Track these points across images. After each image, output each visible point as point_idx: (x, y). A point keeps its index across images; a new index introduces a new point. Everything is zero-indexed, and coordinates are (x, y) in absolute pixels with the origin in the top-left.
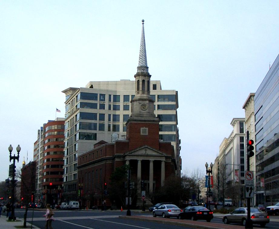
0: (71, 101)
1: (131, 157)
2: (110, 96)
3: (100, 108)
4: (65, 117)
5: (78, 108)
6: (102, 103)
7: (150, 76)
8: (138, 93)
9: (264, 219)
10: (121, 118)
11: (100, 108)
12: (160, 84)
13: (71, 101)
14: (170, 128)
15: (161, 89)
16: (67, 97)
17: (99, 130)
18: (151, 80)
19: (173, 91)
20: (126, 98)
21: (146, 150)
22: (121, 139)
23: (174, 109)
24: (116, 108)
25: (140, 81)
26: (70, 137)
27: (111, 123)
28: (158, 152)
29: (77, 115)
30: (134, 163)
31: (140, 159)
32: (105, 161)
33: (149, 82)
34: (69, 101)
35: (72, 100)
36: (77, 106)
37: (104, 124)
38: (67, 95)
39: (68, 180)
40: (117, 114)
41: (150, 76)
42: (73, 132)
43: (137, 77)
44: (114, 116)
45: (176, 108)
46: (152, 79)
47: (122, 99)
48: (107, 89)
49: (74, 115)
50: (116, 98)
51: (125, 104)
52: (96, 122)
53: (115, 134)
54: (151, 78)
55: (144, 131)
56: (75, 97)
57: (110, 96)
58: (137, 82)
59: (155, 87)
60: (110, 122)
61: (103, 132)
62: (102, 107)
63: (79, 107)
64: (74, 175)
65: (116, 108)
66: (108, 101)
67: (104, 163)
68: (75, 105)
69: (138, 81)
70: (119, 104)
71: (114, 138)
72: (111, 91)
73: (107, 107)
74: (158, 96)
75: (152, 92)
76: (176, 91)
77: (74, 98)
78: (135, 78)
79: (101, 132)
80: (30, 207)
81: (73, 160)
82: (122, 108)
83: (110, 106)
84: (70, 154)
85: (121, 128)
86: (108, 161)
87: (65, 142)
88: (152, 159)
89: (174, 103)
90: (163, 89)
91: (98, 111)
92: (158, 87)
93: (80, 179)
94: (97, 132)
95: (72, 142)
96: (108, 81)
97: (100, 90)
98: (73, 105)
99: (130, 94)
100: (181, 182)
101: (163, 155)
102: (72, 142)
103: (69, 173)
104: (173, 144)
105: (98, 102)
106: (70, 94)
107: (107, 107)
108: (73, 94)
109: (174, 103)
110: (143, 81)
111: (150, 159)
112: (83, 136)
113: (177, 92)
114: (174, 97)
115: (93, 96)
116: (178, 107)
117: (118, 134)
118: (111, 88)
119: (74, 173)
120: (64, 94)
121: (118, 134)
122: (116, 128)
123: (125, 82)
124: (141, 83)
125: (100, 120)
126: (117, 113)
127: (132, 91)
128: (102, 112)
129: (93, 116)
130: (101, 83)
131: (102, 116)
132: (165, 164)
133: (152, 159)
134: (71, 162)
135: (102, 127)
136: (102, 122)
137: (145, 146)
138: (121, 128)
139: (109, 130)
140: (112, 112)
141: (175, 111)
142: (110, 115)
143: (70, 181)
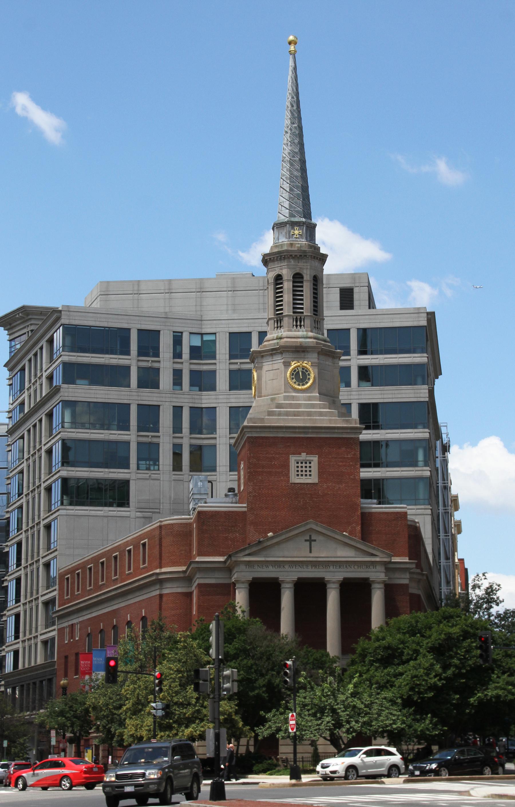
0: (33, 352)
1: (256, 568)
3: (141, 384)
4: (7, 421)
5: (54, 385)
6: (149, 365)
7: (323, 258)
9: (242, 473)
10: (223, 420)
11: (141, 384)
12: (369, 287)
14: (407, 454)
15: (371, 304)
16: (13, 343)
18: (325, 272)
19: (418, 311)
20: (240, 343)
21: (310, 541)
22: (219, 502)
23: (419, 380)
24: (203, 381)
25: (285, 278)
26: (29, 569)
27: (186, 440)
29: (52, 410)
31: (288, 577)
32: (158, 586)
33: (317, 281)
35: (31, 355)
36: (50, 378)
37: (158, 444)
38: (13, 337)
39: (20, 667)
40: (203, 406)
41: (323, 258)
42: (41, 442)
43: (271, 265)
44: (197, 412)
45: (432, 375)
46: (329, 268)
47: (222, 348)
48: (167, 310)
49: (41, 412)
51: (234, 367)
52: (125, 438)
53: (196, 482)
54: (325, 267)
58: (272, 281)
59: (347, 299)
60: (179, 435)
62: (149, 379)
63: (58, 380)
64: (45, 643)
65: (203, 381)
66: (228, 356)
67: (157, 592)
68: (45, 375)
69: (278, 278)
70: (212, 367)
71: (195, 497)
73: (166, 379)
74: (363, 333)
75: (334, 317)
76: (428, 313)
77: (41, 348)
78: (265, 269)
79: (144, 474)
81: (41, 547)
82: (222, 380)
83: (177, 375)
84: (30, 525)
85: (223, 457)
86: (168, 585)
87: (8, 552)
88: (334, 577)
89: (419, 358)
90: (379, 305)
91: (131, 395)
92: (360, 297)
93: (66, 657)
95: (35, 554)
96: (170, 281)
98: (36, 375)
100: (434, 654)
101: (378, 559)
102: (35, 554)
103: (25, 635)
104: (421, 516)
105: (132, 361)
106: (25, 331)
108: (38, 330)
109: (419, 358)
110: (298, 278)
111: (328, 577)
112: (78, 493)
113: (431, 317)
114: (424, 335)
115: (114, 339)
116: (438, 372)
117: (209, 482)
118: (183, 306)
119: (44, 637)
121: (209, 482)
122: (201, 460)
123: (234, 286)
124: (287, 286)
125: (140, 429)
126: (207, 399)
127: (253, 314)
128: (149, 397)
129: (115, 415)
130: (143, 287)
131: (149, 416)
133: (334, 577)
134: (32, 595)
135: (149, 454)
136: (148, 437)
137: (308, 527)
138: (223, 457)
139: (177, 466)
140: (188, 398)
141: (426, 387)
142: (177, 411)
143: (31, 669)
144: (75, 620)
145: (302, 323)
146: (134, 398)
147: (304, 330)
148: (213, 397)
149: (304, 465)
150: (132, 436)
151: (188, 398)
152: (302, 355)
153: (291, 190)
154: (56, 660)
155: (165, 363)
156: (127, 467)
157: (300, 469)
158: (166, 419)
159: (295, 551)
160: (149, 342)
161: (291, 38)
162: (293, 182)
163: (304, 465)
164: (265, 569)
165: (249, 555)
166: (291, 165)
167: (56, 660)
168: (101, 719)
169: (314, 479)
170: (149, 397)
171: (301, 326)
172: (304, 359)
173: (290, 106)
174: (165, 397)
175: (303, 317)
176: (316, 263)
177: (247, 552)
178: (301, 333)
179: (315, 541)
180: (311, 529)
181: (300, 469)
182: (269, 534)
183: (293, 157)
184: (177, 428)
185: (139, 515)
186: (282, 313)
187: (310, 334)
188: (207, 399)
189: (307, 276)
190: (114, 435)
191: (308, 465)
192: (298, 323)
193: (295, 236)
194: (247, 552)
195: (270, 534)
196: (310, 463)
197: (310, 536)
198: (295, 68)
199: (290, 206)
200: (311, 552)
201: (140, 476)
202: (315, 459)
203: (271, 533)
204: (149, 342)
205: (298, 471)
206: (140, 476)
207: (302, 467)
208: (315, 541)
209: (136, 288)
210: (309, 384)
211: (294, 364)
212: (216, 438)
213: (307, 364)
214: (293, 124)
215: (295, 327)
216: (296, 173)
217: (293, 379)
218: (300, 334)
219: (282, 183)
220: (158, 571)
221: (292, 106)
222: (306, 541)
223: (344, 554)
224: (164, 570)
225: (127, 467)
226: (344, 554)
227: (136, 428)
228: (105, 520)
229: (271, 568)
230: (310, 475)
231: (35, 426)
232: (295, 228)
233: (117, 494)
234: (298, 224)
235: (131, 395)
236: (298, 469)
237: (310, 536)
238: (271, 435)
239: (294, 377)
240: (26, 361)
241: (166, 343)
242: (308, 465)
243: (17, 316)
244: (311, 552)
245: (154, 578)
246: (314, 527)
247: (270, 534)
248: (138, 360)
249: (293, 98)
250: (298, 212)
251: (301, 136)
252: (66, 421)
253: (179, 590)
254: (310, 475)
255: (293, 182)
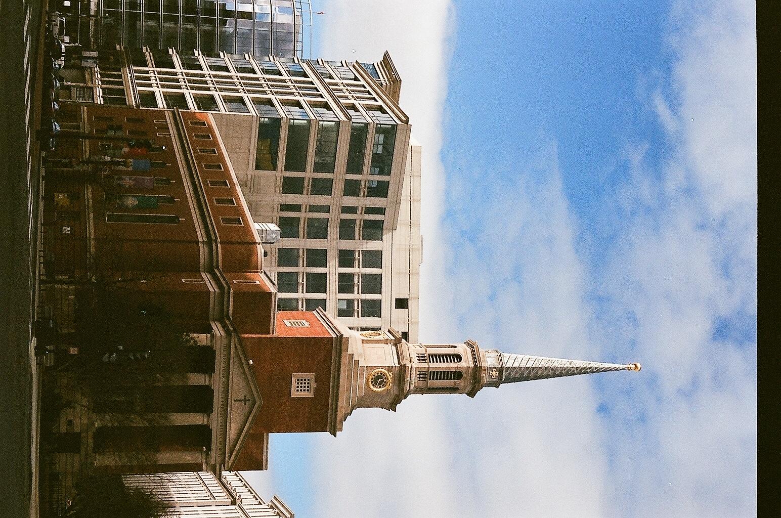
0: (366, 85)
2: (381, 211)
7: (472, 394)
8: (422, 358)
13: (366, 85)
17: (284, 177)
20: (374, 258)
21: (245, 400)
27: (303, 215)
28: (237, 441)
30: (204, 360)
32: (205, 239)
34: (376, 92)
41: (472, 394)
50: (374, 230)
55: (301, 387)
56: (380, 103)
57: (381, 211)
61: (277, 190)
62: (352, 189)
65: (346, 229)
67: (200, 239)
69: (459, 358)
70: (357, 237)
72: (396, 213)
73: (350, 201)
79: (280, 182)
80: (49, 26)
86: (206, 249)
88: (215, 426)
91: (340, 175)
94: (281, 172)
97: (400, 183)
99: (384, 271)
107: (350, 201)
110: (458, 375)
111: (214, 415)
112: (269, 131)
115: (383, 162)
120: (378, 59)
124: (453, 365)
125: (364, 276)
126: (333, 231)
128: (338, 187)
132: (157, 105)
135: (291, 186)
137: (257, 399)
139: (285, 207)
142: (327, 209)
144: (172, 131)
145: (421, 379)
146: (338, 177)
147: (416, 381)
148: (335, 237)
149: (307, 385)
150: (309, 174)
151: (334, 217)
152: (397, 382)
153: (527, 368)
154: (140, 108)
155: (362, 201)
156: (286, 169)
157: (303, 382)
158: (321, 200)
159: (238, 387)
160: (381, 190)
161: (639, 365)
162: (533, 370)
163: (307, 385)
164: (222, 360)
165: (236, 347)
166: (547, 368)
167: (140, 108)
168: (57, 508)
169: (295, 394)
170: (338, 187)
171: (419, 378)
172: (394, 383)
173: (590, 366)
174: (337, 199)
175: (426, 380)
176: (468, 389)
177: (238, 346)
178: (414, 379)
179: (245, 404)
180: (255, 402)
181: (303, 382)
182: (251, 361)
183: (552, 369)
184: (313, 209)
185: (249, 177)
186: (430, 362)
187: (412, 387)
188: (333, 231)
189: (461, 383)
190: (311, 158)
191: (306, 389)
192: (421, 376)
193: (491, 372)
194: (238, 346)
195: (251, 362)
196: (308, 390)
197: (249, 400)
198: (617, 369)
199: (515, 368)
200: (235, 401)
201: (279, 179)
202: (310, 395)
203: (252, 363)
204: (381, 190)
205: (302, 380)
206: (279, 179)
207: (305, 387)
208: (245, 404)
209: (416, 174)
210: (372, 387)
211: (390, 376)
212: (304, 238)
213: (390, 386)
214: (577, 369)
215: (419, 373)
216: (540, 372)
217: (378, 374)
218: (413, 378)
219: (532, 359)
220: (219, 240)
221: (589, 368)
222: (245, 396)
223: (233, 430)
224: (219, 245)
225: (286, 169)
226: (233, 430)
227: (364, 272)
228: (247, 151)
229: (223, 366)
230: (298, 390)
231: (312, 83)
232: (497, 373)
233: (265, 161)
234: (501, 375)
235: (340, 175)
236: (303, 380)
237: (249, 400)
238: (333, 358)
239: (379, 374)
240: (363, 82)
241: (378, 202)
242: (306, 389)
243: (393, 73)
244: (235, 401)
245: (214, 238)
246: (257, 404)
247: (251, 362)
248: (366, 181)
249: (596, 368)
250: (510, 374)
251: (567, 375)
252: (324, 122)
253: (202, 261)
254: (298, 390)
255: (533, 370)
